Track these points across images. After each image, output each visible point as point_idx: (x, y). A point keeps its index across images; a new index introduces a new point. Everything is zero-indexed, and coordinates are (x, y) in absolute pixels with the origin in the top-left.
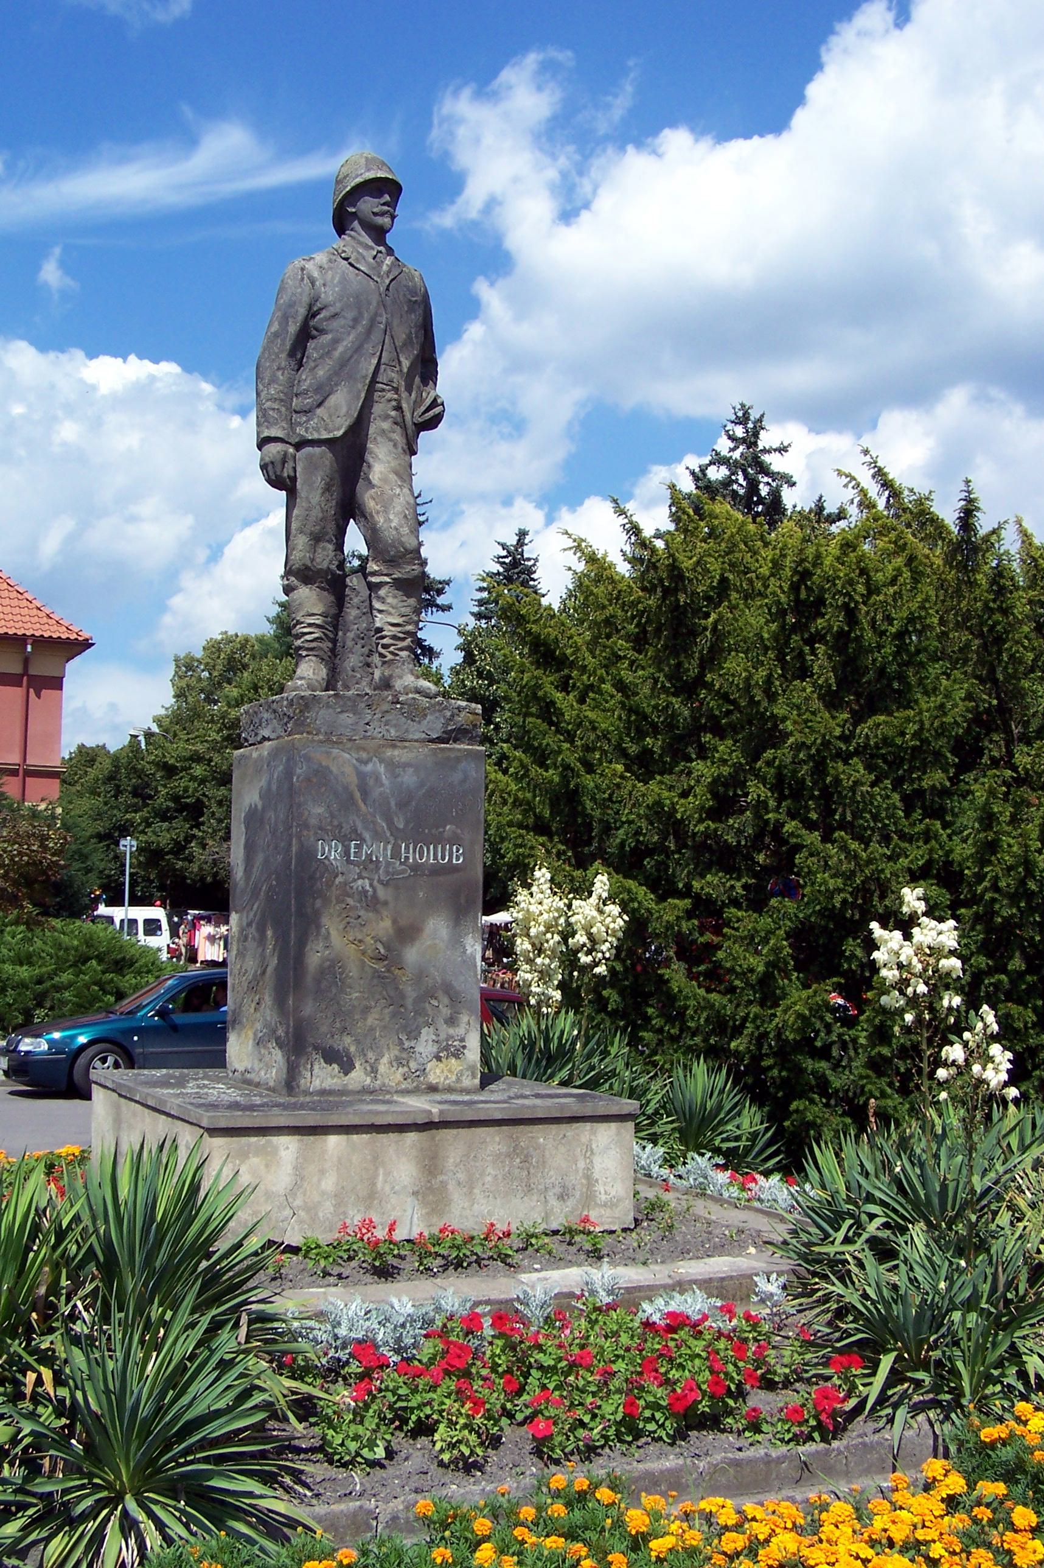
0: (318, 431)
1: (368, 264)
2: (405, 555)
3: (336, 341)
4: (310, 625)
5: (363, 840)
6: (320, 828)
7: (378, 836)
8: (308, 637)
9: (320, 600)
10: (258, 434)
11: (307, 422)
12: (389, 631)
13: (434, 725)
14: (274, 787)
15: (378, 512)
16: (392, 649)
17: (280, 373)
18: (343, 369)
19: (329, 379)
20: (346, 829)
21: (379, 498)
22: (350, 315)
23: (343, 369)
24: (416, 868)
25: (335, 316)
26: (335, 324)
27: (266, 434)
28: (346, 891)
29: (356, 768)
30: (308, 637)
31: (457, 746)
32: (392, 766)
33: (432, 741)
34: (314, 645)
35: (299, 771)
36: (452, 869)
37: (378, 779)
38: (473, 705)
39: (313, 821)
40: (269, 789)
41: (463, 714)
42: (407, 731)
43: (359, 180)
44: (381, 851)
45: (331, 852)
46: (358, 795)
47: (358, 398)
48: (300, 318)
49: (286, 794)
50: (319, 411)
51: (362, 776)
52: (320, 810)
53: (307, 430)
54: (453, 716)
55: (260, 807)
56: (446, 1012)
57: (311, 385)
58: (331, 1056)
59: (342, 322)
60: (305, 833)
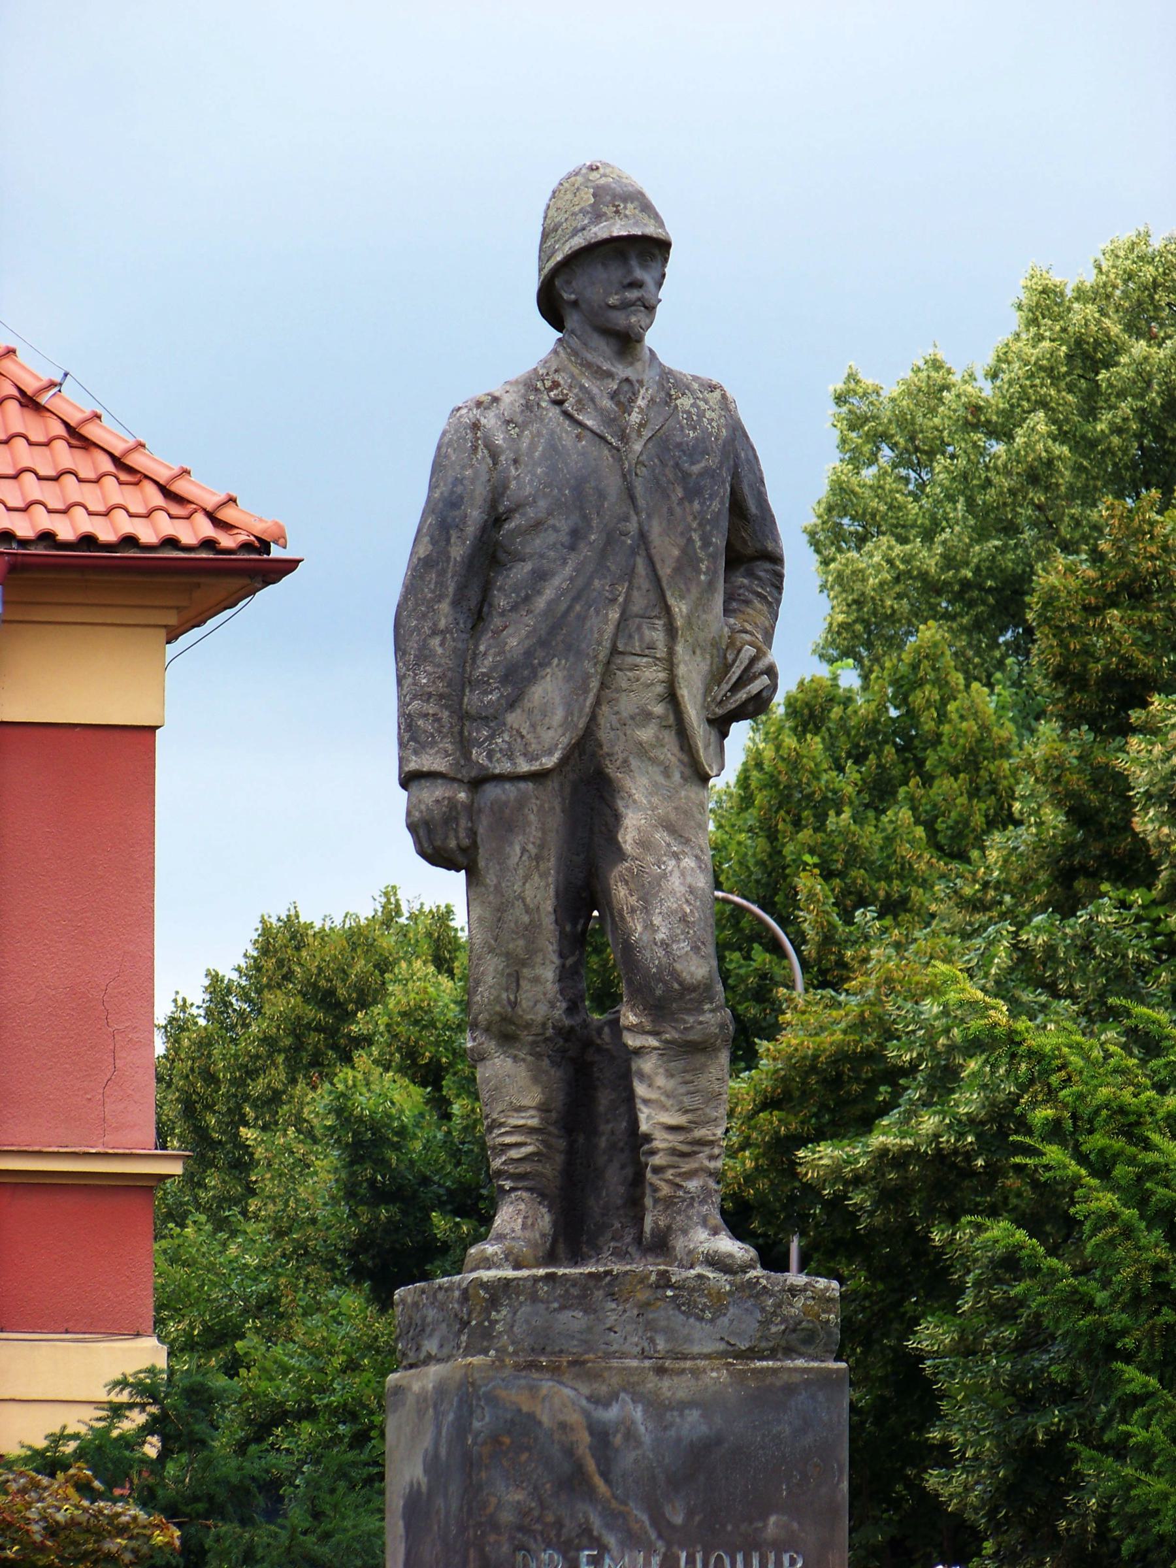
0: (511, 758)
1: (601, 411)
2: (681, 996)
3: (541, 576)
4: (517, 1129)
5: (603, 1549)
6: (521, 1528)
8: (514, 1154)
9: (535, 1080)
10: (400, 768)
11: (492, 737)
12: (662, 1141)
13: (742, 1325)
14: (443, 1451)
15: (633, 911)
16: (669, 1175)
17: (435, 642)
18: (557, 637)
19: (529, 654)
20: (570, 1529)
21: (635, 880)
22: (564, 524)
23: (557, 637)
25: (537, 526)
26: (538, 543)
27: (412, 766)
29: (587, 1414)
30: (514, 1154)
31: (789, 1363)
32: (657, 1408)
33: (740, 1355)
34: (522, 1169)
35: (477, 1425)
37: (630, 1435)
38: (822, 1283)
39: (507, 1517)
40: (436, 1456)
41: (799, 1302)
42: (688, 1339)
43: (578, 242)
46: (591, 1466)
47: (586, 691)
48: (471, 530)
50: (513, 719)
51: (601, 1436)
52: (519, 1496)
53: (490, 756)
54: (779, 1305)
55: (424, 1488)
57: (493, 668)
59: (552, 537)
60: (492, 1538)
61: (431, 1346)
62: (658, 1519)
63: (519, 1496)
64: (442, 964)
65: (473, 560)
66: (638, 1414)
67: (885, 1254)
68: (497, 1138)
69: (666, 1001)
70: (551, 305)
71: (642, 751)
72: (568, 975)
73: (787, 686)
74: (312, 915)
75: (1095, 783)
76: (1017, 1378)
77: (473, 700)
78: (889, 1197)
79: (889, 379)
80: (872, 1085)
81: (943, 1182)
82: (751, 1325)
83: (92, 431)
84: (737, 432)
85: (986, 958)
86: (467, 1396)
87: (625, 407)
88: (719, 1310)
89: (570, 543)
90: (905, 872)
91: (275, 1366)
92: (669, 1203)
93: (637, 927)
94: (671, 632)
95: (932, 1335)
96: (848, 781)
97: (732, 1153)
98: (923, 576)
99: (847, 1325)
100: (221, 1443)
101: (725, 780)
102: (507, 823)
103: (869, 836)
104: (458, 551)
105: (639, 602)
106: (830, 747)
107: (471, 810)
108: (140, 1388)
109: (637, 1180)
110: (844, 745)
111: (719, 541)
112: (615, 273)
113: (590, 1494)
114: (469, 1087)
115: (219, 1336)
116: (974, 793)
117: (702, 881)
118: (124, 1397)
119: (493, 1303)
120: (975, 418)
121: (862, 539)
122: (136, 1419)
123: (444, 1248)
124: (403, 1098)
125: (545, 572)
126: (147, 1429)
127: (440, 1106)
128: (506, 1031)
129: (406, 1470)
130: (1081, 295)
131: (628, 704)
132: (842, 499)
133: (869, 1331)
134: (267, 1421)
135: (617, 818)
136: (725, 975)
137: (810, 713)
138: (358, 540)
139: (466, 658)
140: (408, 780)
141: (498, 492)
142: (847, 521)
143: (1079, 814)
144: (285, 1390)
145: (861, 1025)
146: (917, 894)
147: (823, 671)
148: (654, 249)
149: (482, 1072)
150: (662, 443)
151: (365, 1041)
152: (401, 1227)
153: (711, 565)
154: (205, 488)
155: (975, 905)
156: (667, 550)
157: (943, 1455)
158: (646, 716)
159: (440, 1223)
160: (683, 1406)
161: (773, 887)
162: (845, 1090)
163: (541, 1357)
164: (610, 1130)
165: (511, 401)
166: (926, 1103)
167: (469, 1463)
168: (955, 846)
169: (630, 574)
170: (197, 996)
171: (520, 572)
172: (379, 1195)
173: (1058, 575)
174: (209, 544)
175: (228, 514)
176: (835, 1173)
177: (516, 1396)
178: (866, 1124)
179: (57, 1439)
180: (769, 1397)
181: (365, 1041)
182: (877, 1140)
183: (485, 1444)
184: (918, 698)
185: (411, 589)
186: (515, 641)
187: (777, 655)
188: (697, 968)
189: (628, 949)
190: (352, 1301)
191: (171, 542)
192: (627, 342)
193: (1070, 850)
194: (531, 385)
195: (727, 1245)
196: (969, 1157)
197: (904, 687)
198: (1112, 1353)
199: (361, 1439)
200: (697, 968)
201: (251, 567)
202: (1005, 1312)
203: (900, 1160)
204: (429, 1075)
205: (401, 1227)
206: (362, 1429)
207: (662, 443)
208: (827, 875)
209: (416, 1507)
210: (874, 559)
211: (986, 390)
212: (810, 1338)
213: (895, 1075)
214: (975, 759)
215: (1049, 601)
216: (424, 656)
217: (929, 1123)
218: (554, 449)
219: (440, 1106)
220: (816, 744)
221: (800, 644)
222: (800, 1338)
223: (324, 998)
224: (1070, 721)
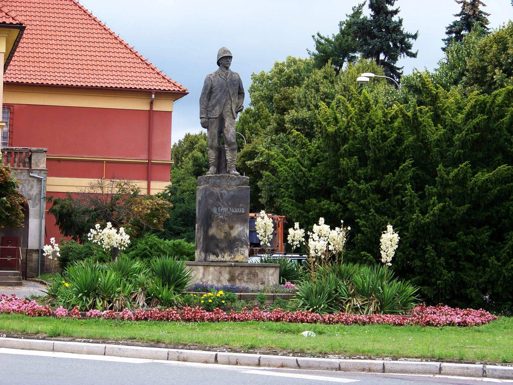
3: (217, 95)
7: (225, 206)
12: (229, 160)
13: (238, 182)
18: (218, 102)
20: (217, 205)
22: (219, 89)
23: (218, 102)
24: (233, 213)
25: (216, 89)
26: (216, 91)
28: (217, 218)
32: (228, 191)
36: (241, 213)
37: (225, 194)
39: (210, 203)
44: (225, 210)
45: (215, 210)
49: (206, 197)
50: (213, 111)
51: (221, 194)
52: (211, 201)
56: (240, 245)
58: (214, 254)
61: (202, 183)
62: (228, 204)
63: (211, 201)
64: (205, 140)
65: (209, 93)
66: (226, 192)
67: (255, 174)
68: (210, 160)
69: (230, 144)
70: (218, 64)
71: (228, 115)
72: (219, 141)
73: (245, 108)
74: (191, 134)
75: (280, 120)
76: (270, 188)
77: (208, 109)
78: (256, 167)
79: (258, 73)
80: (254, 155)
81: (264, 166)
82: (239, 182)
83: (165, 77)
84: (240, 79)
85: (268, 140)
86: (206, 189)
87: (227, 76)
88: (235, 180)
89: (220, 91)
90: (258, 130)
91: (184, 186)
92: (230, 167)
93: (227, 136)
94: (231, 102)
95: (259, 183)
96: (252, 120)
97: (237, 162)
98: (262, 96)
99: (250, 182)
100: (178, 194)
101: (237, 120)
102: (212, 123)
103: (254, 126)
104: (207, 92)
105: (228, 98)
106: (250, 115)
107: (208, 122)
108: (168, 187)
109: (226, 165)
110: (251, 116)
111: (237, 91)
112: (226, 60)
113: (220, 201)
114: (207, 154)
115: (178, 181)
116: (266, 121)
117: (234, 131)
118: (166, 189)
119: (209, 179)
120: (268, 78)
121: (254, 92)
122: (168, 191)
123: (204, 172)
124: (200, 155)
125: (218, 94)
126: (169, 192)
127: (204, 156)
128: (211, 147)
129: (199, 198)
130: (281, 64)
131: (226, 110)
132: (253, 86)
133: (252, 183)
134: (183, 192)
135: (225, 123)
136: (237, 142)
137: (247, 112)
138: (196, 90)
139: (208, 104)
140: (201, 118)
141: (212, 85)
142: (253, 90)
143: (278, 124)
144: (185, 188)
145: (253, 148)
146: (259, 133)
147: (249, 107)
148: (231, 57)
149: (209, 152)
150: (231, 80)
151: (195, 148)
152: (199, 170)
153: (236, 94)
154: (178, 84)
155: (266, 134)
156: (231, 92)
157: (261, 197)
158: (228, 111)
159: (204, 169)
160: (231, 191)
161: (243, 132)
162: (251, 155)
163: (214, 185)
164: (223, 159)
165: (214, 75)
166: (260, 157)
167: (206, 197)
168: (264, 127)
169: (227, 95)
170: (177, 142)
171: (214, 94)
172: (197, 166)
173: (277, 96)
174: (179, 90)
175: (181, 87)
176: (250, 164)
177: (212, 189)
178: (254, 159)
179: (158, 193)
180: (241, 190)
181: (195, 148)
182: (255, 161)
183: (208, 195)
184: (260, 110)
185: (202, 96)
186: (213, 102)
187: (244, 105)
188: (234, 140)
189: (226, 138)
190: (193, 178)
191: (174, 90)
192: (227, 68)
193: (277, 128)
194: (216, 73)
195: (236, 172)
196: (265, 163)
197: (258, 109)
198: (280, 187)
199: (194, 194)
200: (234, 140)
201: (183, 93)
202: (267, 181)
203: (258, 163)
204: (203, 152)
205: (199, 170)
206: (194, 193)
207: (231, 80)
208: (249, 130)
209: (200, 202)
210: (257, 93)
211: (269, 74)
212: (246, 183)
213: (257, 153)
214: (266, 117)
215: (275, 100)
216: (203, 104)
217: (261, 159)
218: (218, 80)
219: (204, 156)
220: (248, 115)
221: (247, 102)
222: (244, 183)
223: (192, 143)
224: (277, 113)
